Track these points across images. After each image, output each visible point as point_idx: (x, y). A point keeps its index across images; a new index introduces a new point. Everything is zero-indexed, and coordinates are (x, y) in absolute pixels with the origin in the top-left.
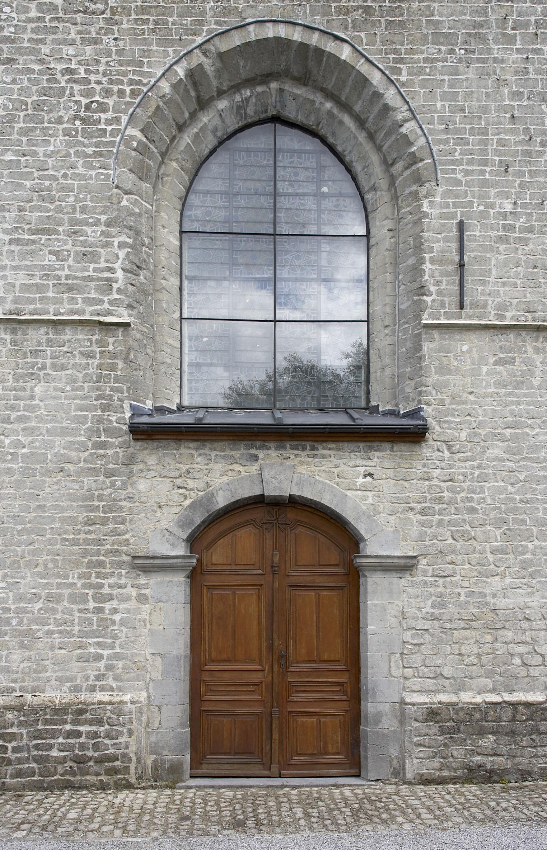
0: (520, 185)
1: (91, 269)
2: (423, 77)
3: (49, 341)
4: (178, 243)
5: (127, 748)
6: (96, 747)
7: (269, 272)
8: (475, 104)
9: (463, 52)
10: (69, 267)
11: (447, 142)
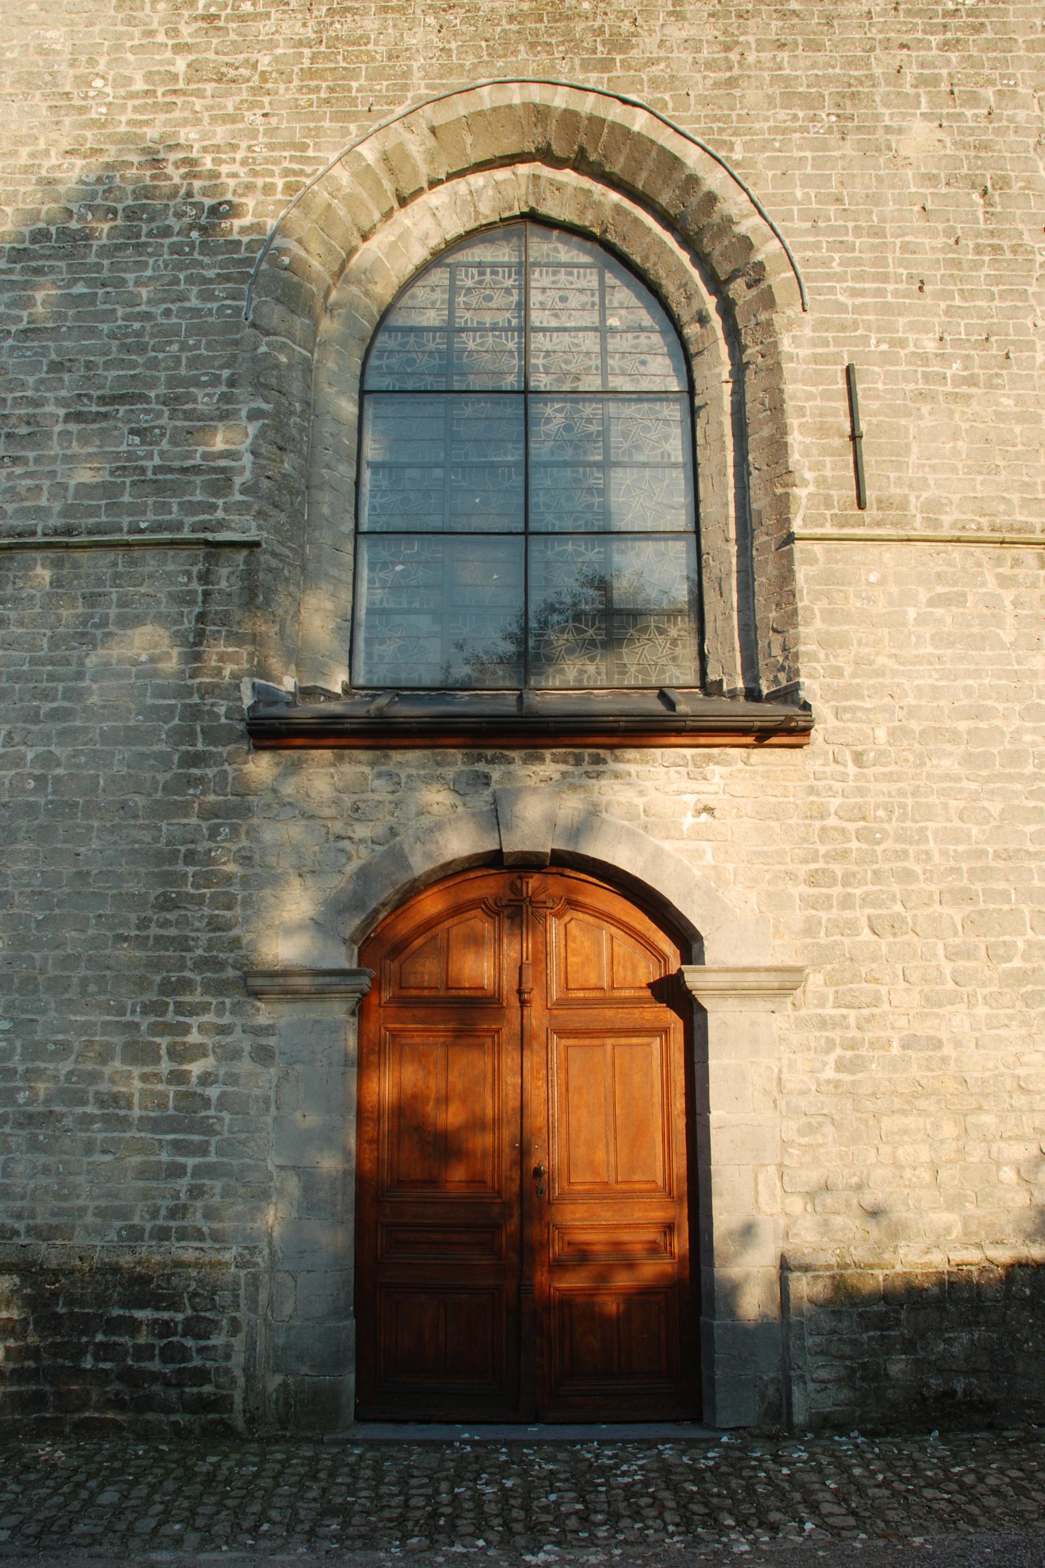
0: (947, 313)
3: (117, 576)
4: (355, 410)
5: (228, 1357)
6: (169, 1353)
8: (859, 190)
9: (833, 118)
10: (162, 454)
11: (817, 246)
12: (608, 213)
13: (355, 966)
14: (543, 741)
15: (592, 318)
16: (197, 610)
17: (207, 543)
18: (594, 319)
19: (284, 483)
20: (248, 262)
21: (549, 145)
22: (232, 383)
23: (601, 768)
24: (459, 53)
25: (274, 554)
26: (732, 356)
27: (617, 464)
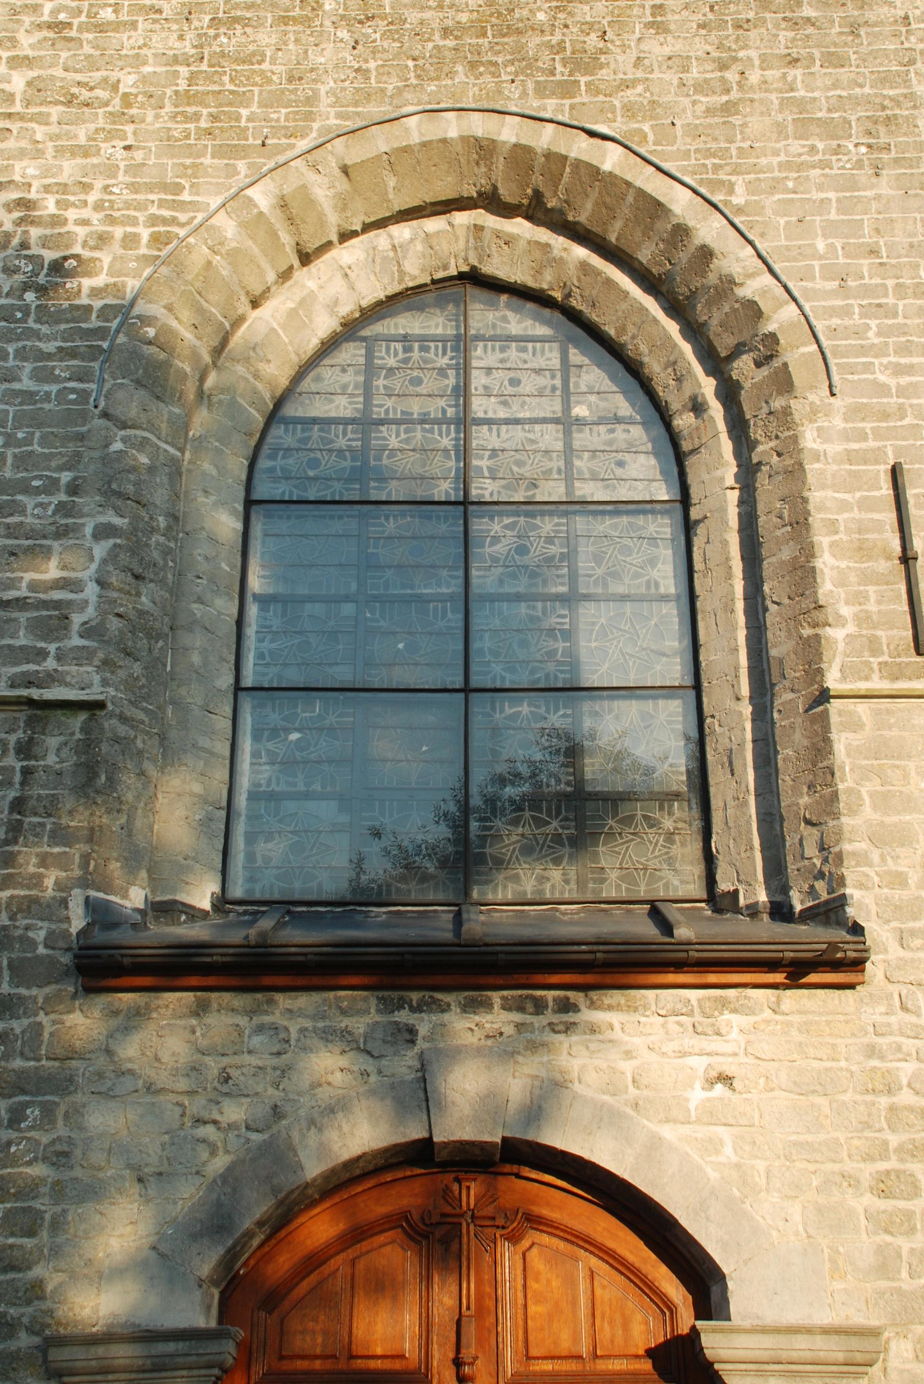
1: (24, 585)
2: (781, 196)
4: (239, 526)
7: (453, 582)
8: (900, 239)
9: (863, 149)
11: (846, 312)
12: (572, 272)
13: (213, 1324)
14: (491, 980)
15: (553, 407)
16: (12, 794)
17: (31, 703)
18: (554, 407)
19: (140, 624)
20: (100, 333)
21: (495, 188)
22: (74, 489)
23: (570, 1017)
24: (379, 74)
25: (123, 719)
26: (737, 454)
27: (587, 597)
